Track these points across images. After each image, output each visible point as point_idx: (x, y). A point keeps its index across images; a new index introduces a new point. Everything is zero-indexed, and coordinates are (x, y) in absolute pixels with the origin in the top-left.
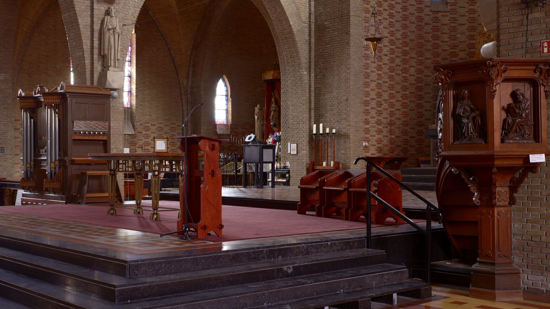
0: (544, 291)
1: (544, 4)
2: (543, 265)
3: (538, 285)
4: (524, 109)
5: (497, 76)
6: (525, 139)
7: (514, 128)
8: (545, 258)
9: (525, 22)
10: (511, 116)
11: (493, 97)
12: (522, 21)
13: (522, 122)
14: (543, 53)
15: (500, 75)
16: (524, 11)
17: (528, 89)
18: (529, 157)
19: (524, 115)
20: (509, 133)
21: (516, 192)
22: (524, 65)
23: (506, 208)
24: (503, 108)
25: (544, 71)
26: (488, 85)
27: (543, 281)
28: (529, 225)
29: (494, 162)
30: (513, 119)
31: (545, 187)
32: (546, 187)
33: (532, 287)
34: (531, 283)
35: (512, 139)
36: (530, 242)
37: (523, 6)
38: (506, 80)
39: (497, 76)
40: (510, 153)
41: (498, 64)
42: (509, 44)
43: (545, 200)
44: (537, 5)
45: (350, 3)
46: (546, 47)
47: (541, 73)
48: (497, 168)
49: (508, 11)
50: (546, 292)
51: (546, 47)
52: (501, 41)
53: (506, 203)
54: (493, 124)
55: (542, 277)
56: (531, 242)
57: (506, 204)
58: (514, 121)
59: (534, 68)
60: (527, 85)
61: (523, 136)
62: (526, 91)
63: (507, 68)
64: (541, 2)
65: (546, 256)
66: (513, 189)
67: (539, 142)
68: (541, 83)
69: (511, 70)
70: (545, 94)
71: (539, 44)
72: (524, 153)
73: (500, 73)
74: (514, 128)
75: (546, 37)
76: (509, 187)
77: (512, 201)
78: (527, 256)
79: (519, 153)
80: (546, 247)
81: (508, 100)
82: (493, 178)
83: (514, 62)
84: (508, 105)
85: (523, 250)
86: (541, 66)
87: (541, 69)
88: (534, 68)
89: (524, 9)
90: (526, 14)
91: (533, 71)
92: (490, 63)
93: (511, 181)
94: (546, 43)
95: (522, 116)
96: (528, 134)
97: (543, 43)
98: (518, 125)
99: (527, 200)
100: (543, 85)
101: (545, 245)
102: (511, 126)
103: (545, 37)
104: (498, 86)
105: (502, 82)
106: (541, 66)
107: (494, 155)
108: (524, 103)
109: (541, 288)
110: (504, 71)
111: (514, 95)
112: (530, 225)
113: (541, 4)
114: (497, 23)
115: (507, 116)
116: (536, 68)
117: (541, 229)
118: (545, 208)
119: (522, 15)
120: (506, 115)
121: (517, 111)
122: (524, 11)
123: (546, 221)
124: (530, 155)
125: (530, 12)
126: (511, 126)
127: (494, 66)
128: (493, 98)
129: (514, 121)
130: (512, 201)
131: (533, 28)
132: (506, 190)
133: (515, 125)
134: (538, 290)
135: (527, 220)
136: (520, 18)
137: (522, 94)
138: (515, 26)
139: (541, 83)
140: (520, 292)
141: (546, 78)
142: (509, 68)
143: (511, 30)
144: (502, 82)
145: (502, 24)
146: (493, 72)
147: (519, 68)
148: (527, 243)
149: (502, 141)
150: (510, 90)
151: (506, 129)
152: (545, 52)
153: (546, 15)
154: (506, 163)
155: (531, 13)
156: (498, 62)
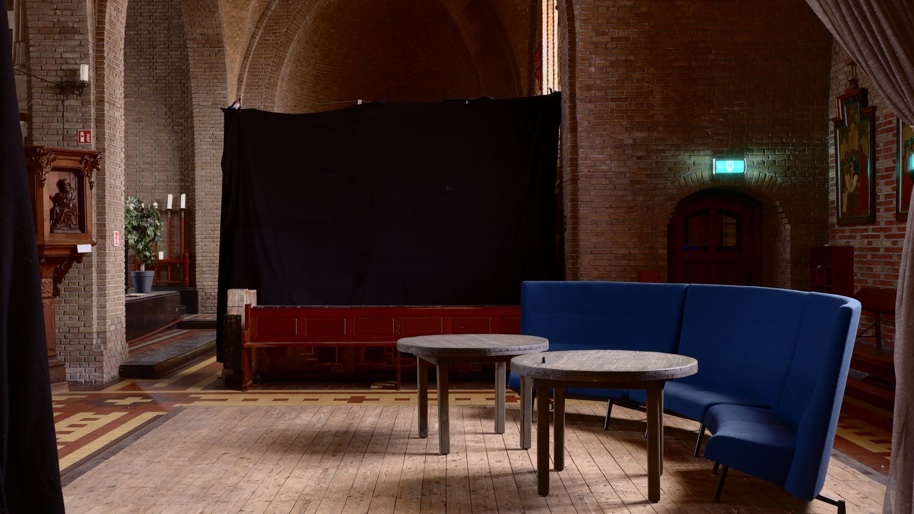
0: (82, 382)
1: (80, 93)
2: (81, 357)
3: (76, 378)
4: (71, 200)
5: (47, 164)
6: (72, 229)
7: (62, 218)
8: (83, 349)
9: (61, 108)
10: (59, 206)
11: (42, 186)
12: (57, 106)
13: (70, 212)
14: (80, 142)
15: (49, 164)
16: (58, 96)
17: (73, 180)
18: (77, 247)
19: (71, 205)
20: (58, 223)
21: (60, 282)
22: (71, 156)
23: (50, 300)
24: (50, 197)
25: (89, 163)
26: (36, 173)
27: (81, 372)
28: (67, 317)
29: (43, 252)
30: (61, 208)
31: (83, 277)
32: (84, 277)
33: (71, 380)
34: (69, 376)
35: (60, 229)
36: (67, 335)
37: (58, 91)
38: (55, 169)
39: (47, 164)
40: (60, 243)
41: (49, 152)
42: (43, 128)
43: (83, 291)
44: (73, 93)
45: (194, 174)
46: (82, 136)
47: (86, 164)
48: (45, 258)
49: (42, 93)
50: (85, 382)
51: (82, 136)
52: (34, 124)
53: (50, 295)
54: (42, 213)
55: (80, 369)
56: (70, 335)
57: (50, 296)
58: (62, 211)
59: (80, 158)
60: (72, 175)
61: (70, 226)
62: (71, 181)
63: (56, 157)
64: (77, 91)
65: (85, 347)
66: (58, 279)
67: (84, 232)
68: (86, 174)
69: (60, 159)
70: (90, 186)
71: (75, 133)
72: (73, 244)
73: (49, 162)
74: (62, 218)
75: (83, 126)
76: (53, 278)
77: (56, 292)
78: (65, 349)
79: (68, 244)
80: (84, 338)
81: (55, 190)
82: (666, 250)
83: (61, 152)
84: (56, 194)
85: (60, 344)
86: (86, 157)
87: (86, 160)
88: (80, 158)
89: (60, 94)
90: (62, 100)
91: (79, 162)
92: (40, 151)
93: (55, 272)
94: (82, 132)
95: (69, 206)
96: (74, 224)
97: (80, 132)
98: (66, 215)
99: (64, 291)
100: (88, 176)
101: (83, 336)
102: (59, 215)
103: (81, 126)
104: (47, 175)
105: (50, 171)
106: (86, 157)
107: (45, 245)
108: (71, 193)
109: (80, 380)
110: (54, 160)
111: (61, 184)
112: (68, 317)
113: (78, 93)
114: (28, 104)
115: (55, 205)
116: (82, 159)
117: (79, 320)
118: (83, 299)
119: (57, 100)
120: (53, 204)
121: (65, 201)
122: (58, 96)
123: (84, 312)
124: (78, 246)
125: (65, 98)
126: (59, 215)
127: (44, 154)
128: (42, 187)
129: (62, 211)
130: (56, 292)
131: (69, 115)
132: (49, 281)
133: (63, 216)
134: (76, 382)
135: (64, 312)
136: (54, 103)
137: (69, 184)
138: (50, 110)
139: (86, 174)
140: (66, 384)
141: (91, 169)
142: (58, 157)
143: (45, 114)
144: (50, 171)
145: (36, 106)
146: (44, 160)
147: (66, 157)
148: (65, 336)
149: (52, 231)
150: (56, 180)
151: (54, 219)
152: (81, 141)
153: (82, 105)
154: (54, 253)
155: (67, 99)
156: (49, 151)
